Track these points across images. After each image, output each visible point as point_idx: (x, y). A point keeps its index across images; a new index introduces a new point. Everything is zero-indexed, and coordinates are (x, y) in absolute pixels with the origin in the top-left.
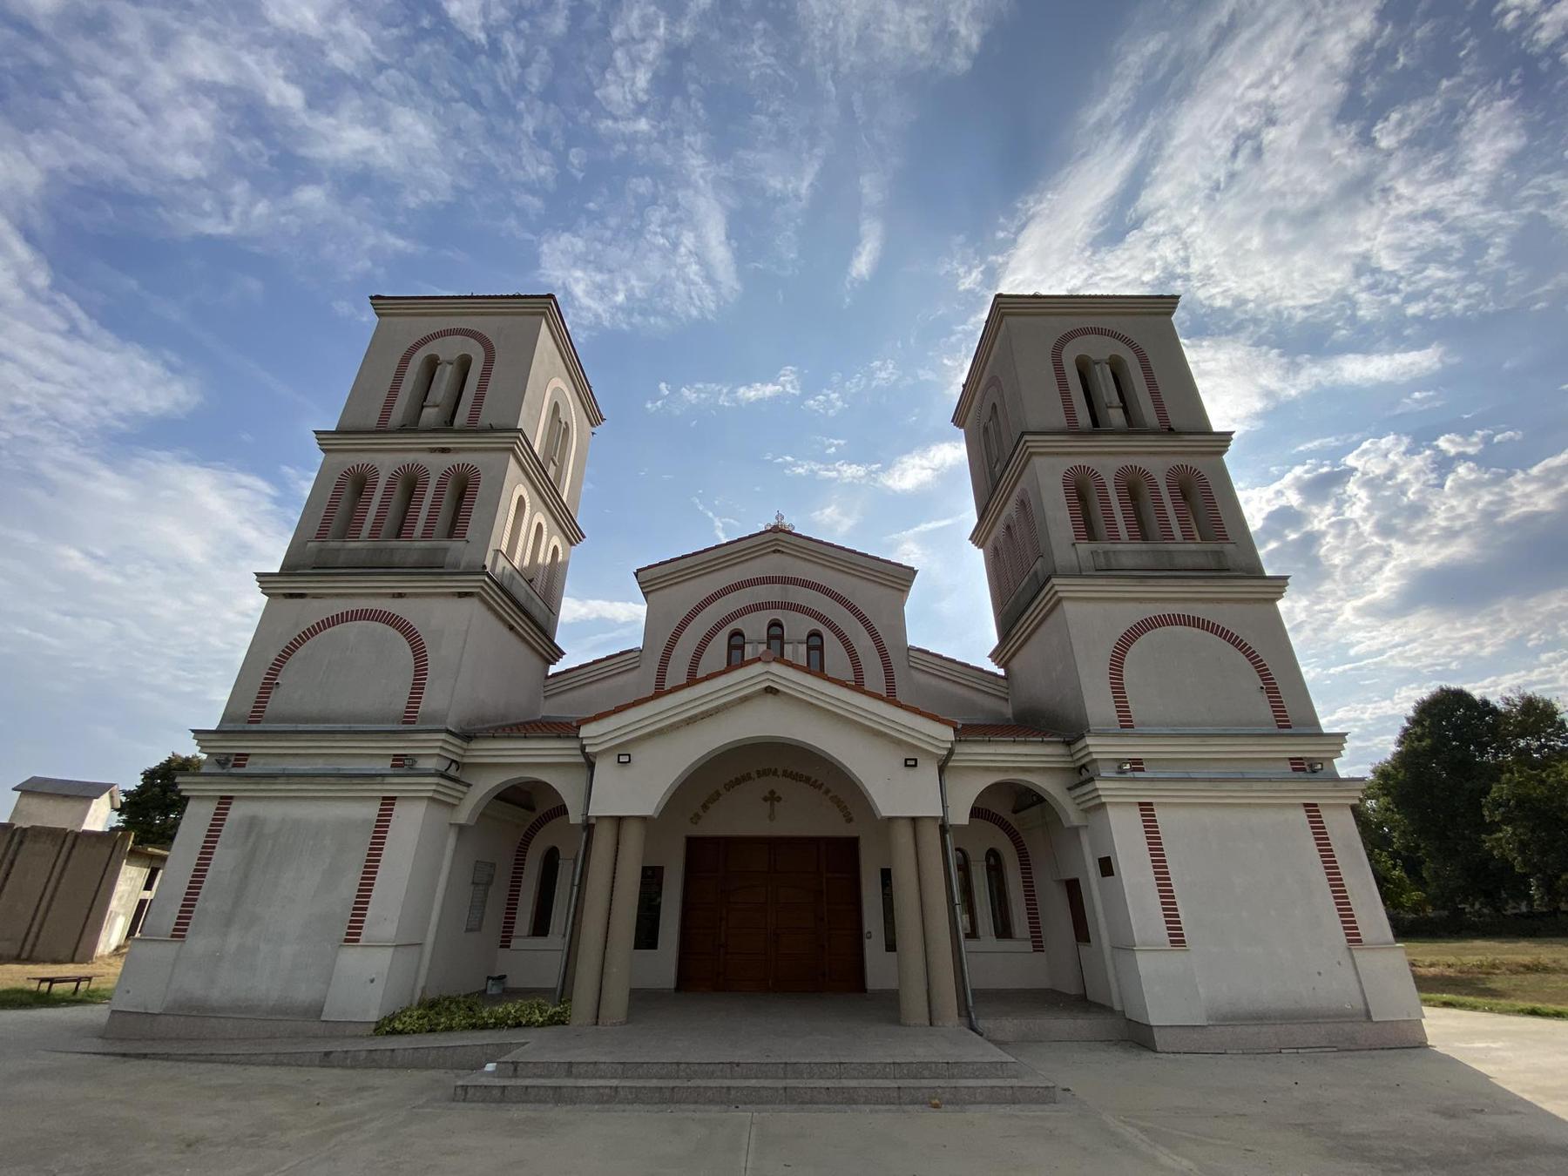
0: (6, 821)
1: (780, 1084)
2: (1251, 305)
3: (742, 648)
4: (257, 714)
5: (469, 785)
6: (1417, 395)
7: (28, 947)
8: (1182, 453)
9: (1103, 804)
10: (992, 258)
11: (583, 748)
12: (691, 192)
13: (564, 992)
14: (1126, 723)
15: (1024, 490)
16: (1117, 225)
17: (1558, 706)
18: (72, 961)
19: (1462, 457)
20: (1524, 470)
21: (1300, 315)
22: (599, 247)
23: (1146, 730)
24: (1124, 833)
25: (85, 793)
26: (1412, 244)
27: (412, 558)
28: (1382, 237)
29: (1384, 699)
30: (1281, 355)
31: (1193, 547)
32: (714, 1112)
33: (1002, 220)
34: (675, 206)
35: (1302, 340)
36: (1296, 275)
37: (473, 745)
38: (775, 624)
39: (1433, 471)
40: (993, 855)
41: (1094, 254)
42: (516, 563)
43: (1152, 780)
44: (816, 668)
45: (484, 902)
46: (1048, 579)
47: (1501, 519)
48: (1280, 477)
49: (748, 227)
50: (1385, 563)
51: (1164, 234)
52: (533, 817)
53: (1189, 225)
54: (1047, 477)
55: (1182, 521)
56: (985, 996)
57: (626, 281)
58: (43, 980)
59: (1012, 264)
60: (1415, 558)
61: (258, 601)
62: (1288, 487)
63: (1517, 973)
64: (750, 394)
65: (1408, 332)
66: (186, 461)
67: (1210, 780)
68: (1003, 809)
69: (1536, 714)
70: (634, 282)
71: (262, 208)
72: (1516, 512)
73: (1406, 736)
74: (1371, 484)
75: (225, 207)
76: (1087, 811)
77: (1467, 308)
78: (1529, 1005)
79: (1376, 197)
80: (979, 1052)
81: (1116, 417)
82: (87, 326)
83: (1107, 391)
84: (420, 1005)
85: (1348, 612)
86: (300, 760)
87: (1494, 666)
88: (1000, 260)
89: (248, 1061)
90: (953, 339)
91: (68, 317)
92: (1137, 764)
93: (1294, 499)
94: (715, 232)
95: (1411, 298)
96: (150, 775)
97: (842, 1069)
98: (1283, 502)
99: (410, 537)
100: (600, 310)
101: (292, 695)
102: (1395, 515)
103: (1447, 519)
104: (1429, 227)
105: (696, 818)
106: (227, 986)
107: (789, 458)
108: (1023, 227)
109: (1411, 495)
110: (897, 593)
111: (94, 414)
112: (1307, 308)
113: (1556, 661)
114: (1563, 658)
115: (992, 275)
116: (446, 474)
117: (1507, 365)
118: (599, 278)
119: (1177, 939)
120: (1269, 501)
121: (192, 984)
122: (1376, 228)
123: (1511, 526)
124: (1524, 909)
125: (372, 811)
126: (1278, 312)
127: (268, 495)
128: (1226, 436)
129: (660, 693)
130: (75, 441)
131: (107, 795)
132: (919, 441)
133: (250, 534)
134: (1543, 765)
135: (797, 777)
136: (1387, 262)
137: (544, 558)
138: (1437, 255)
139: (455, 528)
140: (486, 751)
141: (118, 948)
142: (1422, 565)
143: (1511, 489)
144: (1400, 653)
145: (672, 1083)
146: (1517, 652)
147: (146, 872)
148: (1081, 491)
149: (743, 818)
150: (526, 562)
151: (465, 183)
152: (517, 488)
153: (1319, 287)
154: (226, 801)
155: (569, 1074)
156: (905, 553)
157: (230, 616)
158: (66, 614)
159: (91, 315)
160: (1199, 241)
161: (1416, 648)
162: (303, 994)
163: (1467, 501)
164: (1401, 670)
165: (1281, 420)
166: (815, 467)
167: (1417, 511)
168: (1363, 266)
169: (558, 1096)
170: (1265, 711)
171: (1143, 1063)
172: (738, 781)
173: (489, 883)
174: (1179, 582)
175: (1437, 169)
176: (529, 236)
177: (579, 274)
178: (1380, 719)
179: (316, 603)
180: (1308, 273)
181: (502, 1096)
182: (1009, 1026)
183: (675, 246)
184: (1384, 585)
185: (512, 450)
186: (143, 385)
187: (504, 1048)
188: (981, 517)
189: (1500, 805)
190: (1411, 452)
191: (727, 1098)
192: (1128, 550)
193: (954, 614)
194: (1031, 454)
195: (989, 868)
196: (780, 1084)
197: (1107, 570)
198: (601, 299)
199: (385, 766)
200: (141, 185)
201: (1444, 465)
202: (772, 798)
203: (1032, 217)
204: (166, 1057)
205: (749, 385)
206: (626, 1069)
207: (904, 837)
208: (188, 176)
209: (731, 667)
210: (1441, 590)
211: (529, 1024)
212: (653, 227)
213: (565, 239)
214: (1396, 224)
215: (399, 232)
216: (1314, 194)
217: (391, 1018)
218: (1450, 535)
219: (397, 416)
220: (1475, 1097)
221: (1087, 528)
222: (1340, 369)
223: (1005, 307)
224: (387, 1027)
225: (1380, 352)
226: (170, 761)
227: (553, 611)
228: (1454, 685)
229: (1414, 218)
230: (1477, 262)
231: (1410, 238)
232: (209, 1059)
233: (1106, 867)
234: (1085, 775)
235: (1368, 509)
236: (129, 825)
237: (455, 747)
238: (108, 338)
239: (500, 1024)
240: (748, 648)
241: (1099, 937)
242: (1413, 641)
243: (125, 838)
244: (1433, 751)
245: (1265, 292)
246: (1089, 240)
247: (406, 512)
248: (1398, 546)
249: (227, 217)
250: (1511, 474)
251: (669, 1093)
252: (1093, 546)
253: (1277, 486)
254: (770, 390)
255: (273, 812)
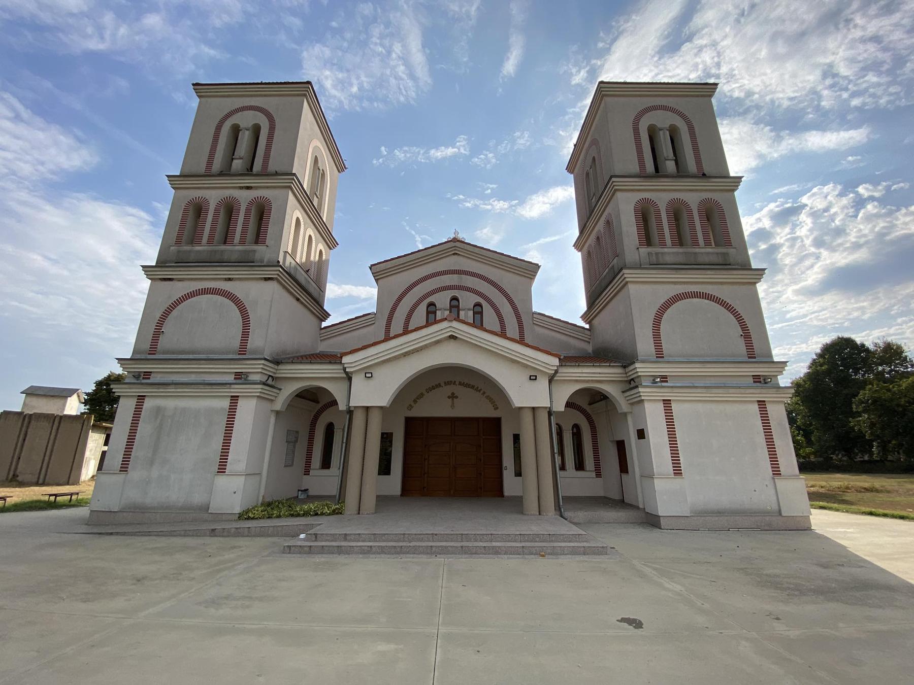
0: (19, 410)
1: (459, 544)
2: (756, 96)
3: (435, 313)
4: (153, 350)
5: (280, 389)
6: (850, 158)
7: (42, 477)
8: (706, 190)
9: (642, 401)
10: (594, 62)
11: (344, 369)
12: (398, 14)
13: (341, 497)
14: (659, 355)
15: (610, 214)
16: (676, 40)
17: (905, 348)
18: (68, 484)
19: (872, 199)
20: (906, 207)
21: (786, 103)
22: (340, 53)
23: (671, 359)
24: (653, 417)
25: (64, 394)
26: (860, 58)
27: (234, 257)
28: (841, 53)
29: (803, 343)
30: (771, 131)
31: (710, 250)
32: (424, 559)
33: (602, 34)
34: (388, 24)
35: (785, 120)
36: (787, 77)
37: (280, 367)
38: (455, 299)
39: (852, 207)
40: (576, 427)
41: (660, 59)
42: (298, 260)
43: (672, 387)
44: (478, 324)
45: (294, 452)
46: (621, 269)
47: (888, 238)
48: (761, 209)
49: (436, 41)
50: (815, 263)
51: (706, 46)
52: (320, 406)
53: (722, 40)
54: (624, 206)
55: (705, 235)
56: (570, 500)
57: (358, 78)
58: (51, 495)
59: (606, 66)
60: (833, 260)
61: (146, 284)
62: (764, 216)
63: (860, 492)
64: (438, 154)
65: (850, 117)
66: (96, 199)
67: (705, 387)
68: (583, 403)
69: (892, 353)
70: (363, 78)
71: (123, 31)
72: (897, 234)
73: (814, 363)
74: (815, 215)
75: (100, 30)
76: (632, 404)
77: (889, 102)
78: (868, 510)
79: (841, 26)
80: (565, 528)
81: (670, 166)
82: (25, 113)
83: (666, 149)
84: (262, 504)
85: (789, 293)
86: (182, 375)
87: (870, 325)
88: (599, 63)
89: (172, 534)
90: (567, 117)
91: (12, 109)
92: (664, 378)
93: (767, 223)
94: (415, 43)
95: (854, 95)
96: (99, 384)
97: (492, 537)
98: (760, 225)
99: (232, 244)
100: (342, 98)
101: (171, 338)
102: (827, 234)
103: (857, 237)
104: (872, 47)
105: (410, 407)
106: (155, 496)
107: (461, 197)
108: (615, 40)
109: (837, 222)
110: (528, 280)
111: (36, 170)
112: (791, 99)
113: (906, 322)
114: (911, 321)
115: (593, 73)
116: (251, 203)
117: (906, 141)
118: (340, 75)
119: (678, 472)
120: (751, 225)
121: (134, 495)
122: (839, 47)
123: (893, 242)
124: (866, 458)
125: (226, 403)
126: (772, 101)
127: (147, 220)
128: (739, 179)
129: (387, 338)
130: (28, 188)
131: (75, 396)
132: (541, 185)
133: (139, 244)
134: (891, 381)
135: (467, 386)
136: (844, 70)
137: (314, 257)
138: (874, 66)
139: (259, 238)
140: (287, 370)
141: (93, 477)
142: (837, 265)
143: (897, 219)
144: (816, 318)
145: (401, 544)
146: (885, 317)
147: (103, 436)
148: (644, 214)
149: (436, 407)
150: (304, 260)
151: (250, 9)
152: (295, 212)
153: (800, 85)
154: (141, 398)
155: (345, 540)
156: (532, 256)
157: (134, 293)
158: (38, 293)
159: (27, 107)
160: (728, 51)
161: (825, 314)
162: (198, 499)
163: (870, 226)
164: (816, 326)
165: (767, 171)
166: (478, 202)
167: (840, 232)
168: (829, 72)
169: (340, 550)
170: (741, 348)
171: (655, 534)
172: (433, 388)
173: (296, 441)
174: (703, 272)
175: (882, 8)
176: (294, 46)
177: (327, 73)
178: (799, 354)
179: (180, 284)
180: (794, 75)
181: (310, 551)
182: (581, 515)
183: (389, 53)
184: (813, 276)
185: (290, 187)
186: (65, 153)
187: (312, 526)
188: (581, 232)
189: (863, 402)
190: (841, 195)
191: (431, 552)
192: (671, 252)
193: (561, 292)
194: (616, 190)
195: (573, 434)
196: (459, 544)
197: (657, 264)
198: (343, 90)
199: (231, 378)
200: (46, 18)
201: (860, 203)
202: (453, 396)
203: (620, 34)
204: (124, 534)
205: (437, 149)
206: (375, 537)
207: (527, 418)
208: (75, 11)
209: (428, 324)
210: (845, 280)
211: (322, 514)
212: (374, 40)
213: (317, 49)
214: (853, 44)
215: (211, 44)
216: (803, 22)
217: (247, 511)
218: (856, 246)
219: (217, 166)
220: (840, 558)
221: (647, 239)
222: (806, 140)
223: (605, 91)
224: (244, 516)
225: (832, 130)
226: (109, 376)
227: (322, 290)
228: (846, 335)
229: (863, 40)
230: (898, 72)
231: (859, 54)
232: (148, 534)
233: (641, 434)
234: (633, 384)
235: (811, 230)
236: (91, 411)
237: (271, 368)
238: (39, 121)
239: (306, 514)
240: (439, 313)
241: (634, 471)
242: (824, 310)
243: (89, 419)
244: (828, 373)
245: (766, 87)
246: (657, 50)
247: (228, 227)
248: (824, 253)
249: (102, 38)
250: (898, 210)
251: (399, 549)
252: (650, 249)
253: (758, 215)
254: (450, 151)
255: (170, 404)
